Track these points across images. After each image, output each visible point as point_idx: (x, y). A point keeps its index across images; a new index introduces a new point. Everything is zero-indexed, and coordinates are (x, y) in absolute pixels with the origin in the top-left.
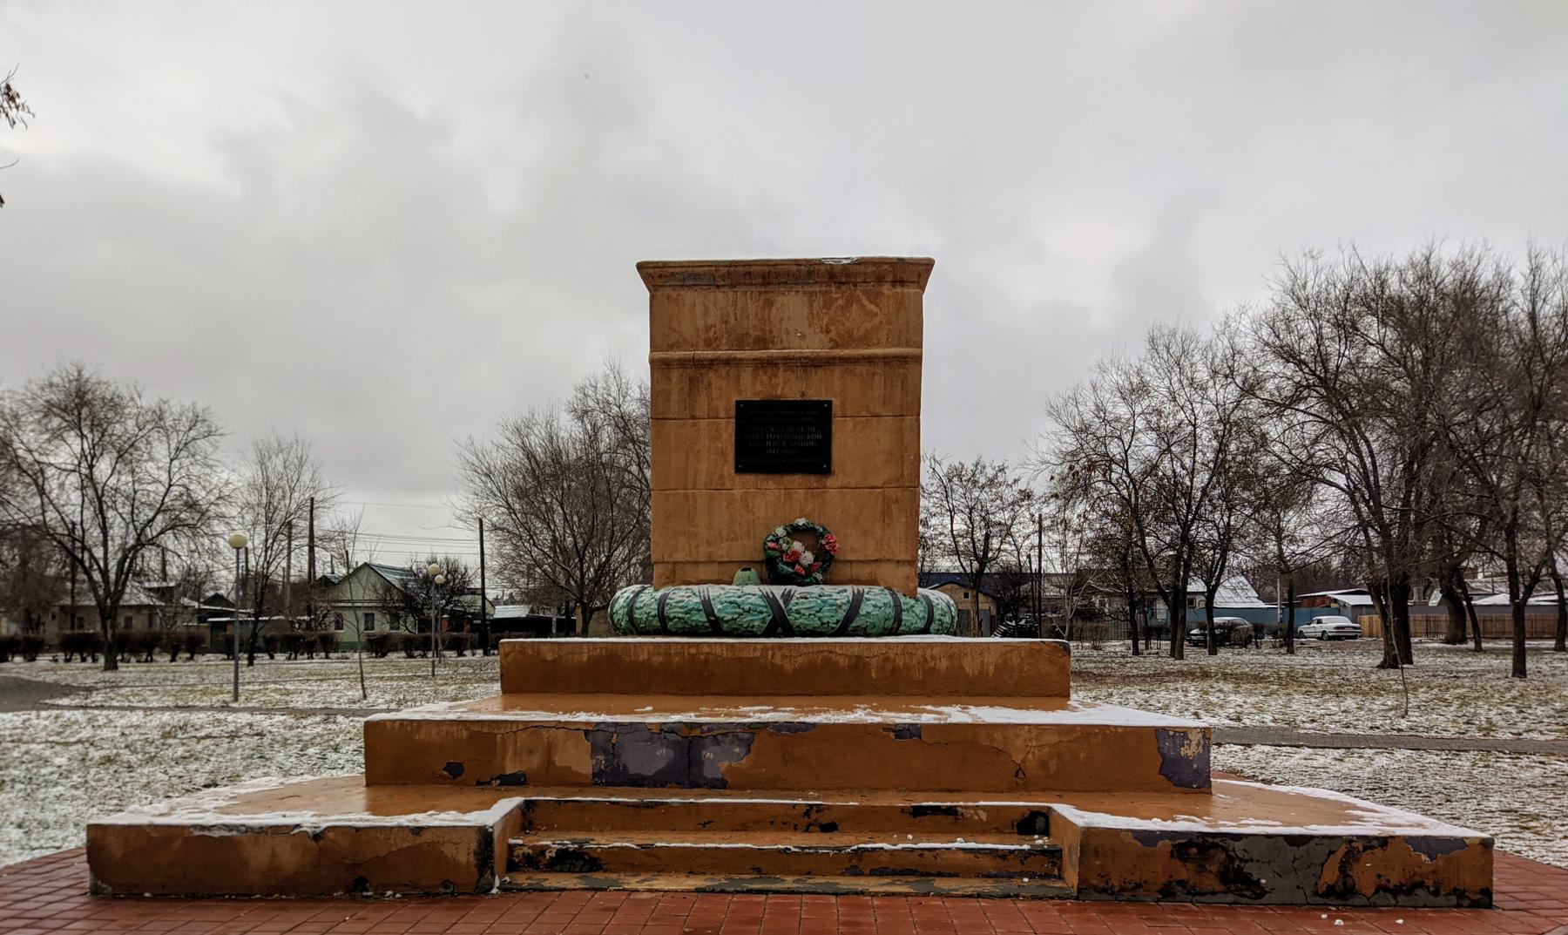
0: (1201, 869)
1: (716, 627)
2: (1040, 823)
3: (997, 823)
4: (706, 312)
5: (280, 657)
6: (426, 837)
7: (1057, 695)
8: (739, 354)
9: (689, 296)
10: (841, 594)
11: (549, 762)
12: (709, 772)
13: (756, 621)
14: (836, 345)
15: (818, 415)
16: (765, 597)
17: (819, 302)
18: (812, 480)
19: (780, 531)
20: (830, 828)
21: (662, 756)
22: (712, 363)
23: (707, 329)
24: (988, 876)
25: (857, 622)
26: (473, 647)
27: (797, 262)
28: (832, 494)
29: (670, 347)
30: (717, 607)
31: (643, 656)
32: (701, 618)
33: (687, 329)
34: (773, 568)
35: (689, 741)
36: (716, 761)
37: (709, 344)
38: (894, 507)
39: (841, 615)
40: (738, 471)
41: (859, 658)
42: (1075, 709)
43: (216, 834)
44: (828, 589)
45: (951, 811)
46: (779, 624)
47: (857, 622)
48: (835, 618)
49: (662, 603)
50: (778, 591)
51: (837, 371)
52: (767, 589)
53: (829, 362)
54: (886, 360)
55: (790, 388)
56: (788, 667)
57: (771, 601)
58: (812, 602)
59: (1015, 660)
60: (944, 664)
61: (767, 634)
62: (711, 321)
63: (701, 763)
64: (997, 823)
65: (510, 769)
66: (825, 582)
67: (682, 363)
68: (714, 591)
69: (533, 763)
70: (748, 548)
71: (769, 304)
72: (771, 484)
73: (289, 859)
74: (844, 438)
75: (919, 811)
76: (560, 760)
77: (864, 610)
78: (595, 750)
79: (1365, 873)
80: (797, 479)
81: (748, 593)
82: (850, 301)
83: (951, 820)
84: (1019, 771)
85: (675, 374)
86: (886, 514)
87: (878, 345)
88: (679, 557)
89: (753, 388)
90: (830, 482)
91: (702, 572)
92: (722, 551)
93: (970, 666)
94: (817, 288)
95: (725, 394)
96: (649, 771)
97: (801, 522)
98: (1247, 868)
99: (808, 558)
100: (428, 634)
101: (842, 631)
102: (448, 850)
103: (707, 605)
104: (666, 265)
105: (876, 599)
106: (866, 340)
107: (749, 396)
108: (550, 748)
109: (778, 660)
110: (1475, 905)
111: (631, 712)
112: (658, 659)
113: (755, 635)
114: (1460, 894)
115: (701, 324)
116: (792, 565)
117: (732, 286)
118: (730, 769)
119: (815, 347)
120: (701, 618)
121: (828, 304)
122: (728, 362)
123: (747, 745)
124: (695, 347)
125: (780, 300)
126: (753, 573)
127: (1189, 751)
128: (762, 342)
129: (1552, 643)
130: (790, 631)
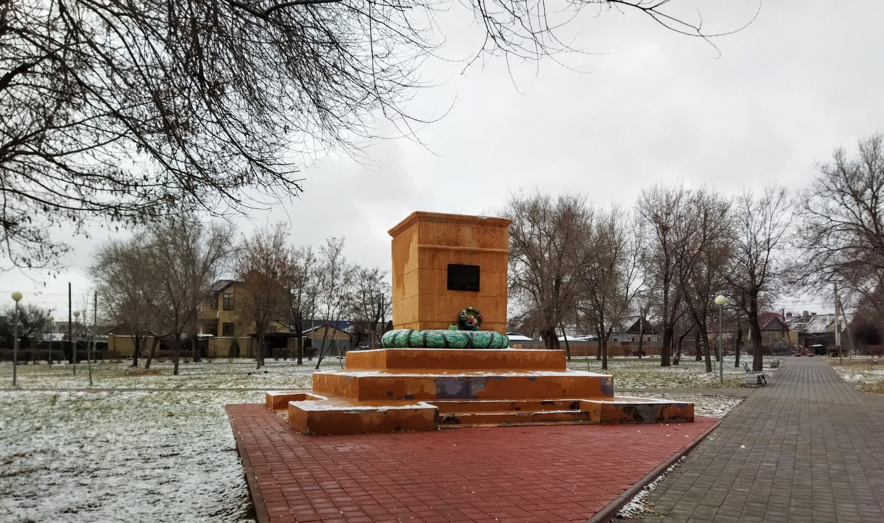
0: (629, 414)
1: (447, 345)
2: (576, 405)
3: (564, 406)
4: (438, 231)
5: (31, 363)
6: (418, 412)
7: (563, 368)
8: (450, 247)
9: (432, 225)
10: (488, 334)
11: (422, 391)
12: (474, 393)
13: (462, 343)
14: (481, 247)
15: (475, 271)
16: (464, 334)
17: (475, 231)
18: (473, 293)
19: (464, 311)
20: (518, 409)
21: (459, 388)
22: (440, 250)
23: (438, 237)
24: (570, 421)
25: (493, 344)
26: (59, 359)
27: (470, 217)
28: (480, 299)
29: (425, 243)
30: (448, 338)
31: (435, 355)
32: (442, 342)
33: (431, 237)
34: (462, 324)
35: (467, 382)
36: (475, 389)
37: (439, 243)
38: (499, 304)
39: (488, 342)
40: (448, 289)
41: (505, 356)
42: (568, 372)
43: (352, 413)
44: (484, 332)
45: (552, 403)
46: (470, 344)
47: (493, 344)
48: (486, 342)
49: (425, 336)
50: (468, 332)
51: (481, 255)
52: (465, 332)
53: (480, 252)
54: (497, 253)
55: (466, 261)
56: (482, 359)
57: (467, 336)
58: (481, 337)
59: (550, 357)
60: (530, 358)
61: (464, 348)
62: (439, 235)
63: (470, 390)
64: (564, 406)
65: (409, 394)
66: (480, 330)
67: (430, 249)
68: (445, 332)
69: (416, 391)
70: (453, 317)
71: (459, 230)
72: (459, 294)
73: (376, 420)
74: (484, 279)
75: (544, 403)
76: (425, 390)
77: (495, 339)
78: (437, 386)
79: (666, 415)
80: (468, 293)
81: (453, 333)
82: (485, 232)
83: (552, 406)
84: (564, 391)
85: (427, 253)
86: (497, 306)
87: (495, 248)
88: (428, 319)
89: (453, 260)
90: (479, 294)
91: (435, 325)
92: (443, 317)
93: (537, 359)
94: (474, 226)
95: (445, 261)
96: (454, 394)
97: (471, 308)
98: (640, 413)
99: (475, 321)
100: (21, 351)
101: (487, 348)
102: (426, 416)
103: (444, 336)
104: (425, 213)
105: (497, 336)
106: (491, 246)
107: (453, 262)
108: (422, 386)
109: (479, 357)
110: (690, 422)
111: (440, 374)
112: (440, 356)
113: (460, 348)
114: (687, 418)
115: (436, 235)
116: (471, 323)
117: (446, 222)
118: (480, 392)
119: (474, 247)
120: (442, 342)
121: (478, 232)
122: (446, 250)
123: (485, 384)
124: (433, 243)
125: (463, 229)
126: (456, 326)
127: (608, 384)
128: (457, 244)
129: (595, 357)
130: (472, 347)
